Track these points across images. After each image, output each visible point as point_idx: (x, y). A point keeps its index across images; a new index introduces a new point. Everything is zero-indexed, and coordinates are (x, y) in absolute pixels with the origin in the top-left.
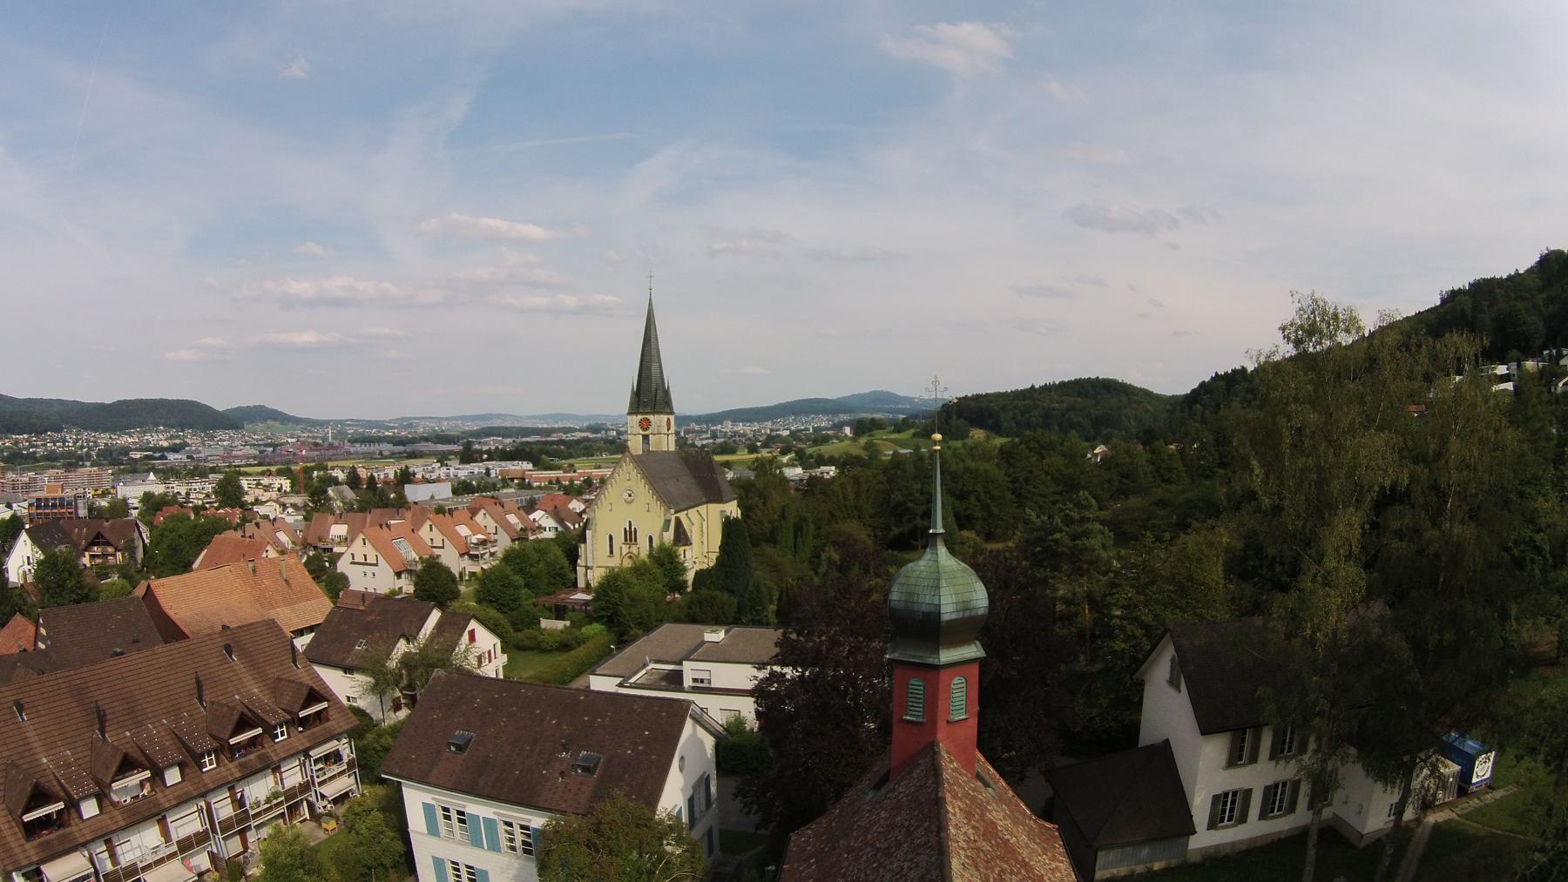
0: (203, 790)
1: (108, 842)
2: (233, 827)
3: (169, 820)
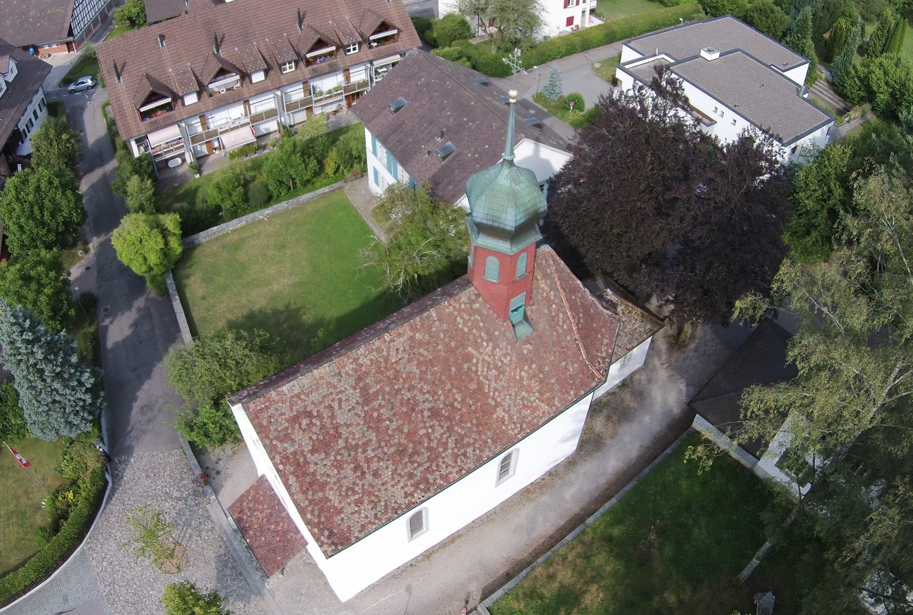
0: (278, 86)
1: (202, 117)
2: (298, 107)
3: (351, 72)
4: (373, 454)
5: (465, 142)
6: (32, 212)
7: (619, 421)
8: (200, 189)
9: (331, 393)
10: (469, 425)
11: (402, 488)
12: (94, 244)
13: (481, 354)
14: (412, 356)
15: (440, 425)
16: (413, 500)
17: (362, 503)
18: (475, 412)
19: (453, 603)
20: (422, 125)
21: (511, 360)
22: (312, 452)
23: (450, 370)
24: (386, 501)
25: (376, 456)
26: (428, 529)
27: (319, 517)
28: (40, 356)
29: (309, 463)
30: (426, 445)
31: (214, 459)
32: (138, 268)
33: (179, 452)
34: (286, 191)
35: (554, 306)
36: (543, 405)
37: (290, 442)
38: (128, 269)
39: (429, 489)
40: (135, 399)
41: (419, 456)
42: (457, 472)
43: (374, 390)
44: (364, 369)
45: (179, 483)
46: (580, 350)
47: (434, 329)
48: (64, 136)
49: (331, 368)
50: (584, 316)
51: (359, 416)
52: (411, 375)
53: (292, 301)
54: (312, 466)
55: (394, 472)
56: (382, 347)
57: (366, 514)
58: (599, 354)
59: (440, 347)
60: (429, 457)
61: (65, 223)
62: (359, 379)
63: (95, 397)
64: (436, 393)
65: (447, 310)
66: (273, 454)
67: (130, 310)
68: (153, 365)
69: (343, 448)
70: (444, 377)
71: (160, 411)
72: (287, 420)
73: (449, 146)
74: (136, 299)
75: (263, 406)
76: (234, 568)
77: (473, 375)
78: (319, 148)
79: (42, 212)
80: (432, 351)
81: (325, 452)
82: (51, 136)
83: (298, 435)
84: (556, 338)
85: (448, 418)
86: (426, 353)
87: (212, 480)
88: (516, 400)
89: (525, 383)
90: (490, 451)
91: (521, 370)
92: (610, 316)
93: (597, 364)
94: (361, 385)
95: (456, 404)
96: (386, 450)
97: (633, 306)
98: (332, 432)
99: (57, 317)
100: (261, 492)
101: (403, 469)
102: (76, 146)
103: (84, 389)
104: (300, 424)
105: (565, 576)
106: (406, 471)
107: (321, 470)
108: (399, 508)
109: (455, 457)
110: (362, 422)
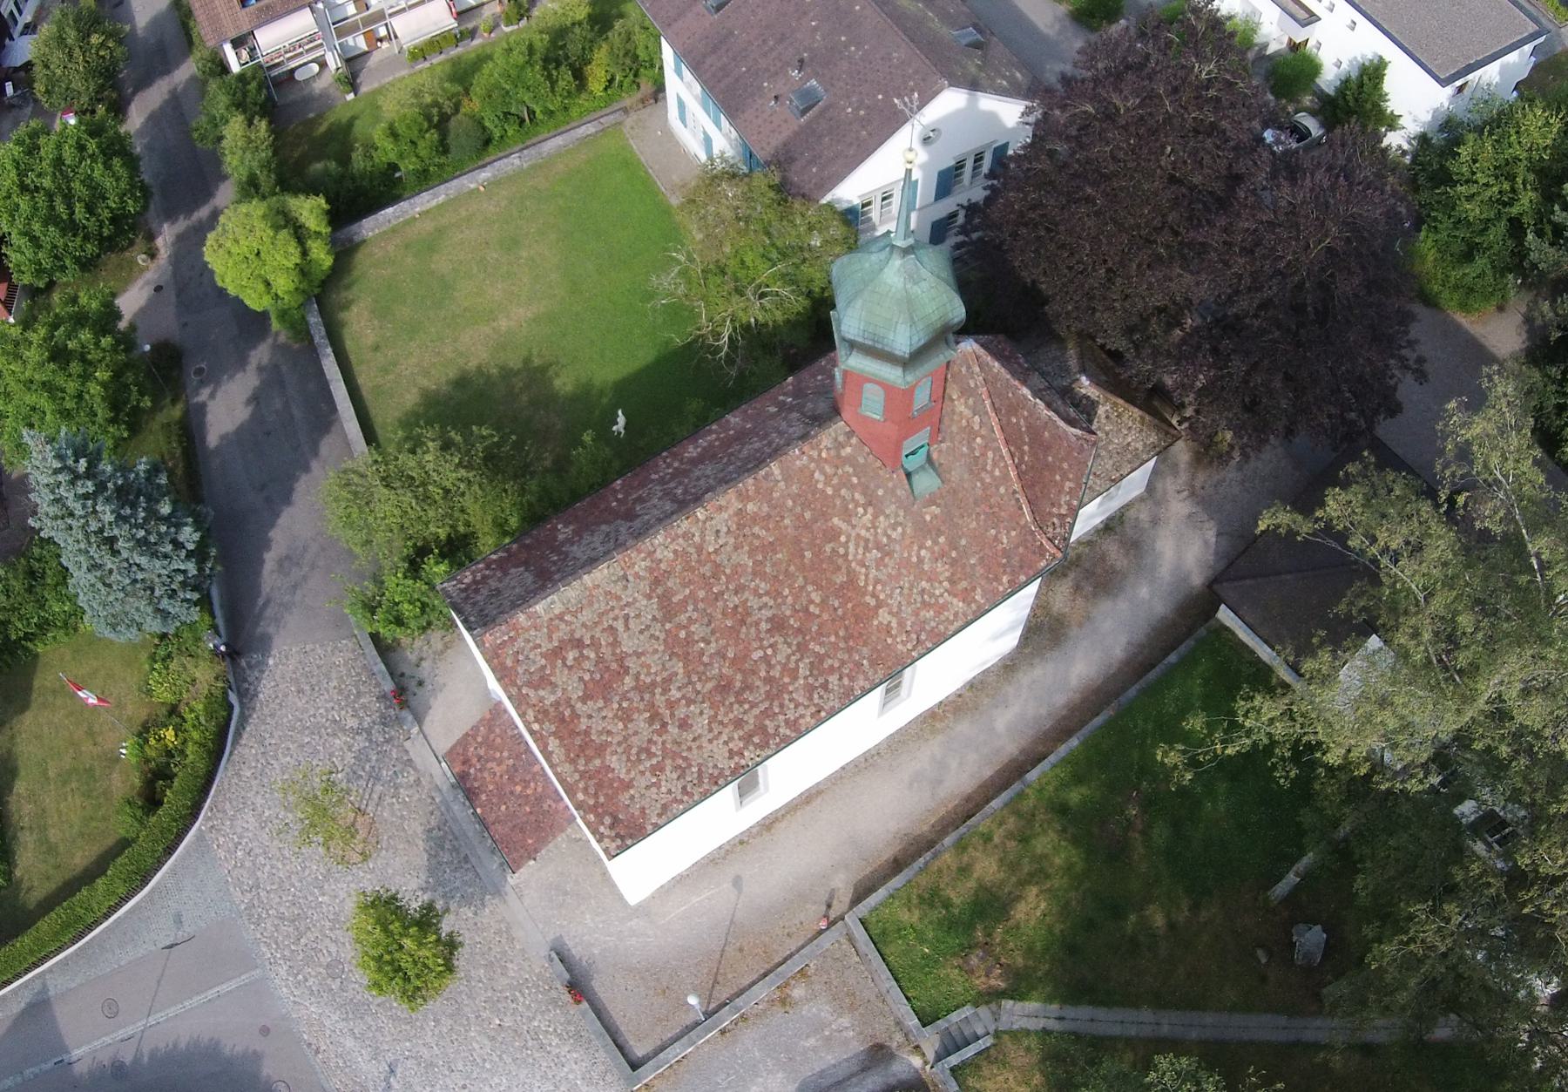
4: (678, 695)
5: (841, 84)
6: (52, 208)
7: (1095, 595)
8: (357, 122)
9: (613, 608)
10: (833, 639)
11: (726, 743)
12: (165, 240)
13: (854, 527)
14: (741, 539)
15: (786, 642)
16: (743, 762)
17: (662, 770)
18: (843, 618)
19: (808, 906)
20: (764, 41)
21: (904, 533)
22: (584, 699)
23: (803, 556)
24: (699, 765)
25: (684, 697)
26: (767, 789)
27: (596, 796)
28: (109, 517)
29: (578, 717)
30: (763, 674)
31: (413, 657)
32: (256, 301)
33: (350, 645)
34: (517, 128)
35: (979, 440)
36: (955, 601)
37: (549, 688)
38: (238, 302)
39: (767, 743)
40: (266, 544)
41: (751, 692)
42: (812, 716)
43: (680, 597)
44: (663, 566)
45: (354, 702)
46: (1021, 508)
47: (775, 495)
48: (95, 39)
49: (612, 571)
50: (1031, 448)
51: (657, 639)
52: (740, 570)
53: (535, 352)
54: (584, 720)
55: (713, 719)
56: (693, 530)
57: (669, 786)
58: (1055, 510)
59: (787, 522)
60: (768, 694)
61: (114, 220)
62: (657, 582)
63: (201, 561)
64: (779, 594)
65: (798, 462)
66: (523, 708)
67: (244, 371)
68: (293, 478)
69: (633, 689)
70: (792, 568)
71: (313, 567)
72: (543, 655)
73: (813, 89)
74: (255, 347)
75: (506, 638)
76: (456, 850)
77: (840, 561)
78: (574, 49)
79: (70, 207)
80: (774, 529)
81: (604, 698)
82: (69, 41)
83: (561, 677)
84: (980, 492)
85: (799, 631)
86: (763, 533)
87: (411, 698)
88: (910, 596)
89: (926, 567)
90: (867, 679)
91: (921, 548)
92: (1079, 438)
93: (1050, 529)
94: (660, 591)
95: (812, 608)
96: (699, 686)
97: (1127, 405)
98: (614, 666)
99: (121, 415)
100: (497, 730)
101: (726, 714)
102: (118, 52)
103: (183, 554)
104: (564, 659)
105: (987, 868)
106: (731, 716)
107: (597, 725)
108: (721, 774)
109: (810, 689)
110: (661, 648)
